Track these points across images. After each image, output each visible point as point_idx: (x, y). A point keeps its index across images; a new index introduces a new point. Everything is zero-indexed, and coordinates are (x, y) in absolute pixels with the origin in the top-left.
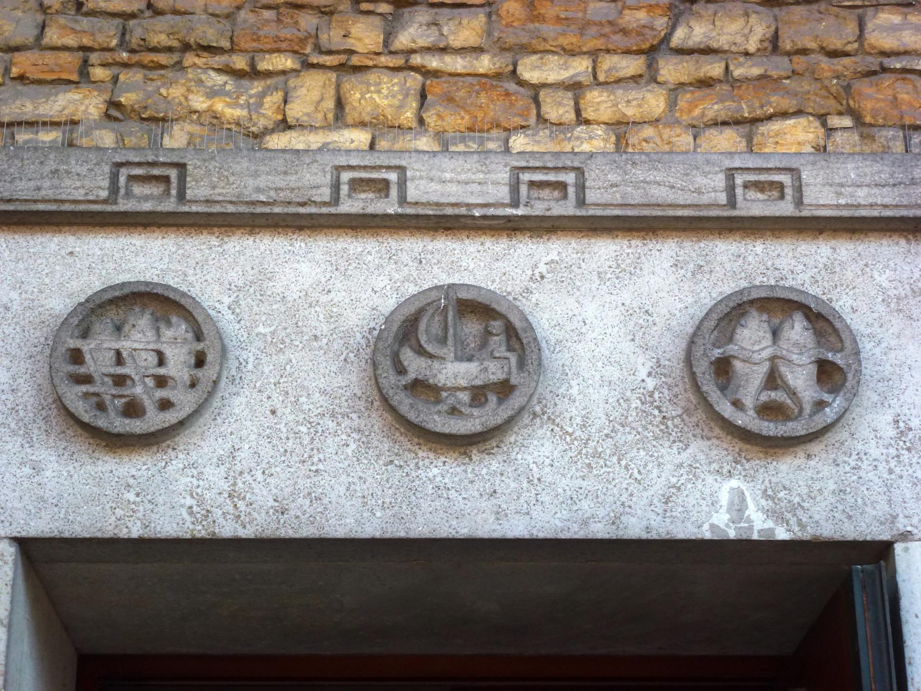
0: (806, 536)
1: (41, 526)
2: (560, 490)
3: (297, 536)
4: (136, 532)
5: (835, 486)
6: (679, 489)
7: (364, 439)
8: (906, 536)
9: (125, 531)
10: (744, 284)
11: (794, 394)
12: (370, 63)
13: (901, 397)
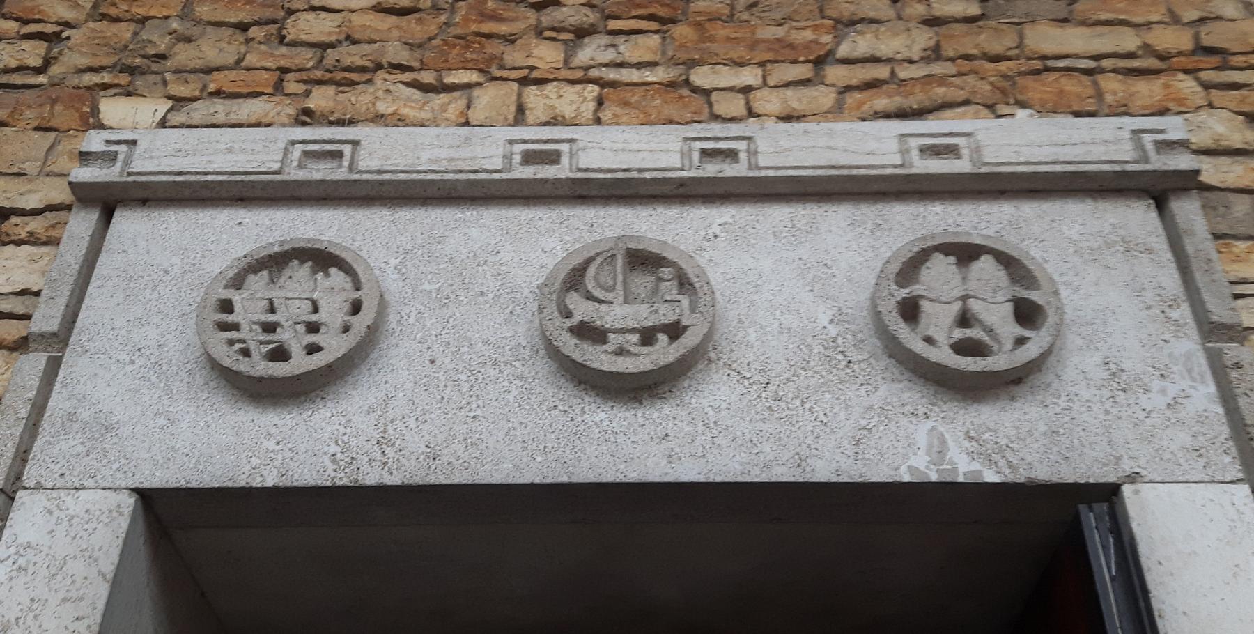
0: (1020, 478)
2: (739, 433)
3: (449, 482)
5: (1046, 428)
6: (870, 430)
7: (527, 386)
8: (1133, 478)
9: (259, 479)
11: (991, 331)
12: (551, 77)
13: (1109, 340)
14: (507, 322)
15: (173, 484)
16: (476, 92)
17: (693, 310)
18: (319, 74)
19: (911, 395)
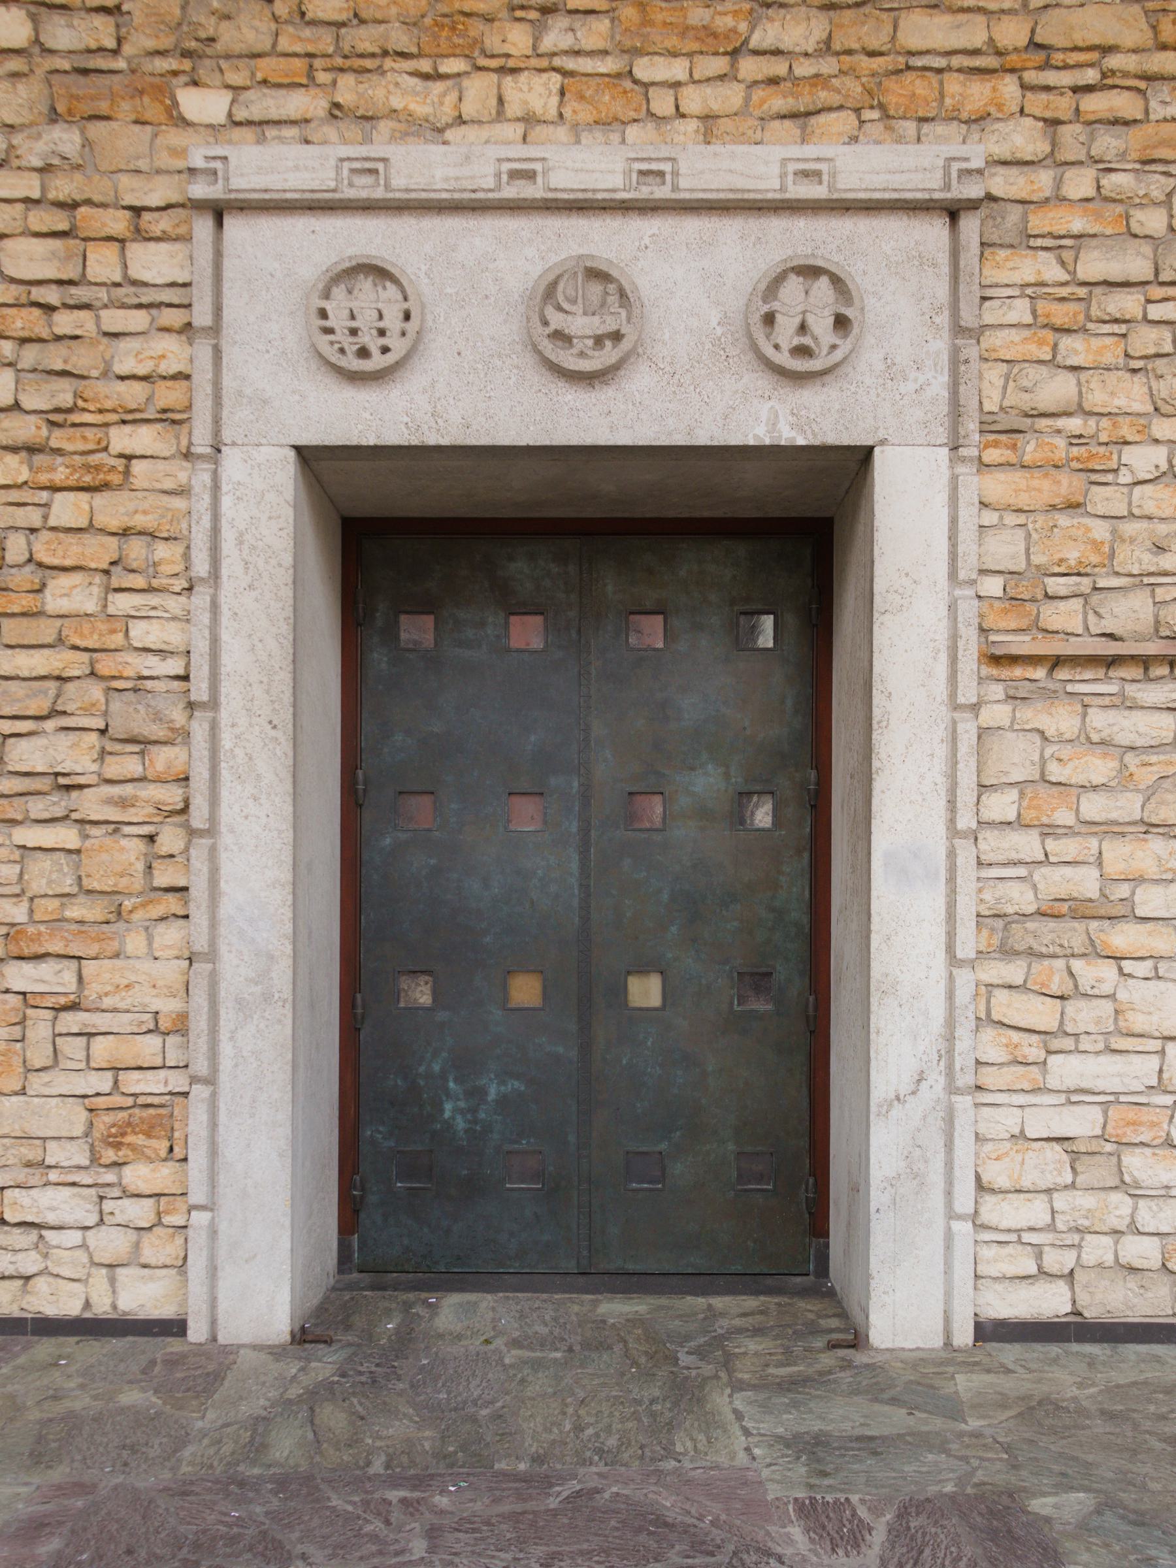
1: (311, 437)
4: (372, 442)
8: (883, 442)
10: (790, 252)
12: (523, 65)
14: (505, 321)
15: (315, 443)
16: (466, 83)
17: (629, 321)
18: (339, 61)
19: (763, 381)
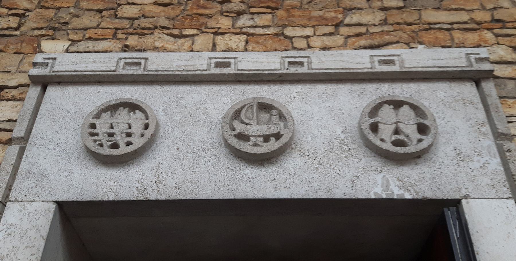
0: (420, 197)
2: (304, 178)
3: (185, 198)
5: (431, 176)
6: (358, 177)
7: (217, 159)
8: (466, 197)
9: (107, 197)
11: (408, 136)
12: (227, 32)
13: (456, 140)
14: (209, 133)
15: (71, 199)
16: (196, 38)
17: (285, 128)
18: (131, 30)
19: (375, 163)
